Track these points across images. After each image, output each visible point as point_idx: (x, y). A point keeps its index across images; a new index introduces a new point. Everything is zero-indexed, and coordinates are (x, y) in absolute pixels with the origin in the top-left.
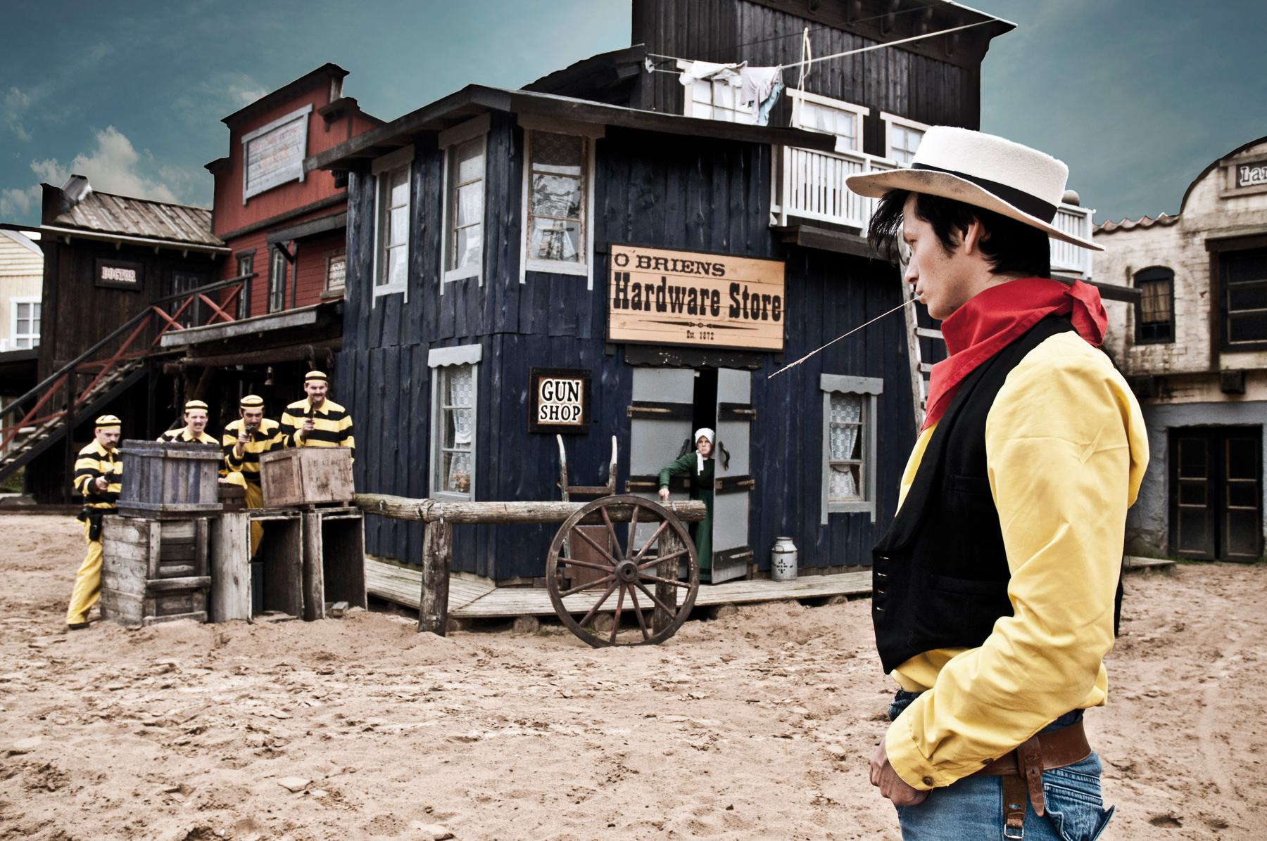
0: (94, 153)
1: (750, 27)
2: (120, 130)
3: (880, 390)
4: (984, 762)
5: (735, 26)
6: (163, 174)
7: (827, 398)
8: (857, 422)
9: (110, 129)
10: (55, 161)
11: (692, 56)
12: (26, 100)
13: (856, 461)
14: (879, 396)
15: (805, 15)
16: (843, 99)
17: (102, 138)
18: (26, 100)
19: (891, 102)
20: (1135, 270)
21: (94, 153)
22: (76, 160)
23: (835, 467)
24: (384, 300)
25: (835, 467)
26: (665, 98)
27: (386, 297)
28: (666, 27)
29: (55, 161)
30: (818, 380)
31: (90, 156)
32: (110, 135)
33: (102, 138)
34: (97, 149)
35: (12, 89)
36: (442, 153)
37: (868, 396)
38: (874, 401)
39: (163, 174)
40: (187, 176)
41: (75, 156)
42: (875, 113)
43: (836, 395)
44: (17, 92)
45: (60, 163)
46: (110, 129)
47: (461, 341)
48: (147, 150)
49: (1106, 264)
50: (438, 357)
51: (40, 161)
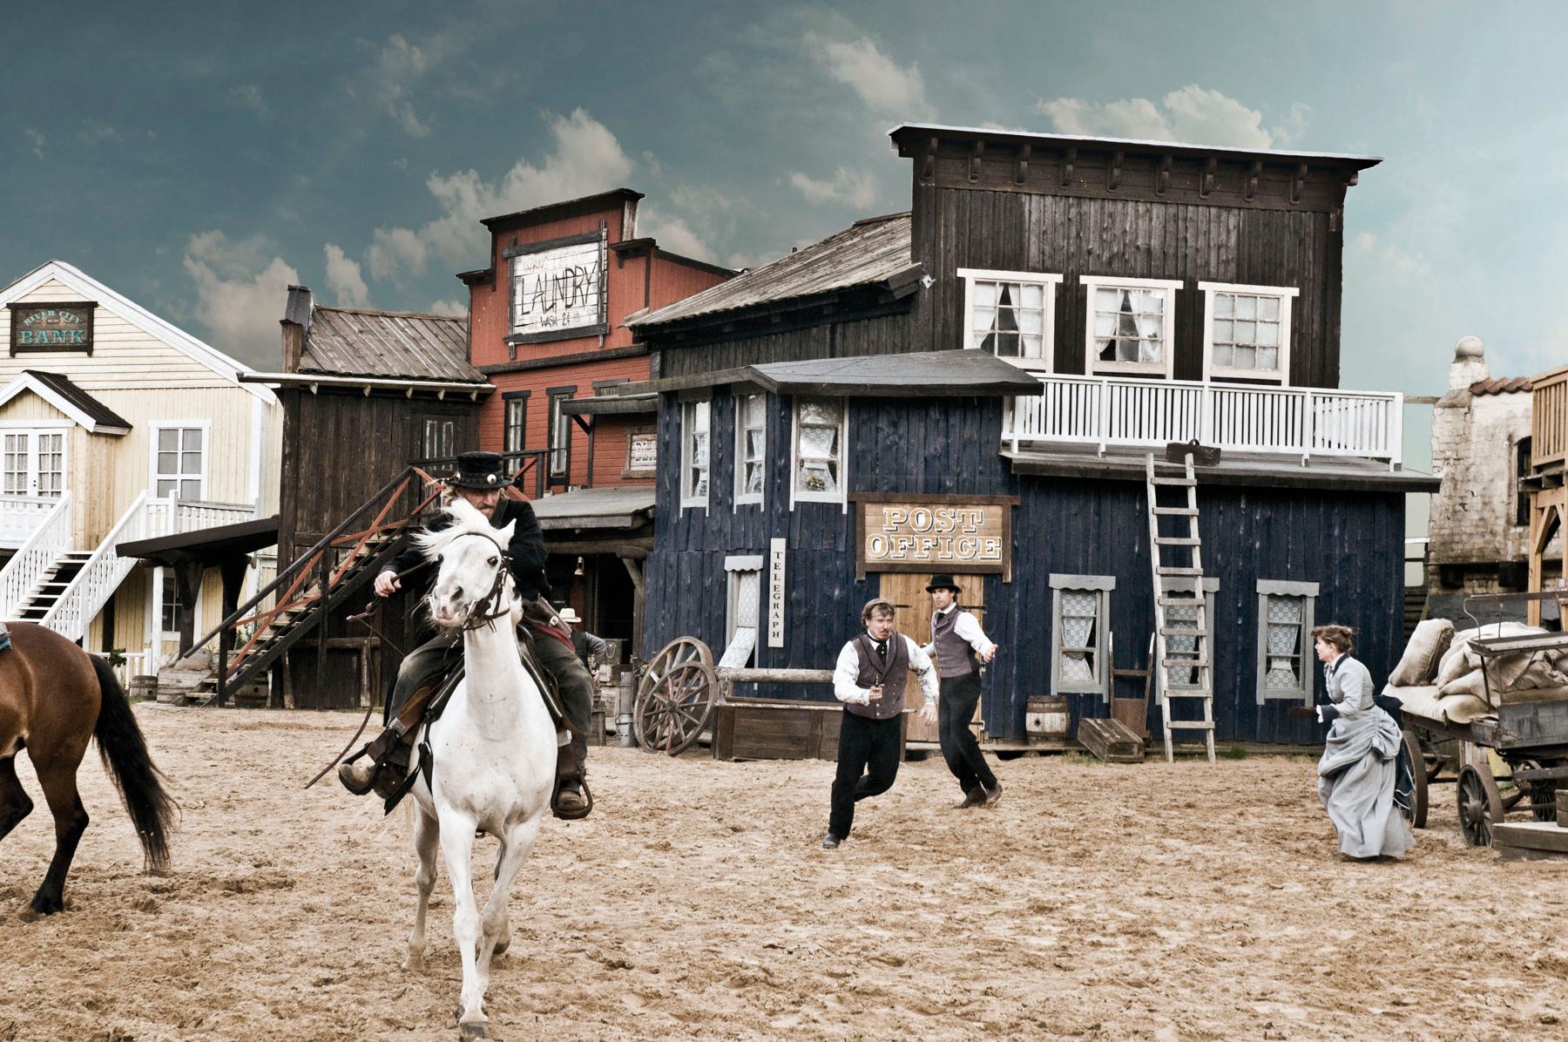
0: (549, 159)
1: (1039, 221)
2: (598, 116)
3: (1113, 587)
4: (516, 597)
5: (1022, 223)
6: (678, 199)
7: (1056, 594)
8: (1092, 614)
9: (578, 114)
10: (473, 174)
11: (975, 264)
12: (419, 60)
13: (1090, 649)
14: (1112, 592)
15: (1104, 194)
16: (1149, 276)
17: (563, 131)
18: (419, 60)
19: (1213, 270)
20: (1516, 440)
21: (549, 159)
22: (513, 173)
23: (1070, 654)
24: (689, 511)
25: (1070, 654)
26: (945, 307)
27: (691, 509)
28: (946, 237)
29: (473, 174)
30: (1047, 578)
31: (540, 166)
32: (578, 125)
33: (563, 131)
34: (554, 152)
35: (393, 38)
36: (680, 406)
37: (1303, 598)
38: (1106, 596)
39: (678, 199)
40: (725, 204)
41: (513, 166)
42: (1191, 284)
43: (1066, 591)
44: (402, 43)
45: (484, 178)
46: (578, 114)
47: (748, 552)
48: (648, 155)
49: (1491, 431)
50: (732, 563)
51: (445, 176)
